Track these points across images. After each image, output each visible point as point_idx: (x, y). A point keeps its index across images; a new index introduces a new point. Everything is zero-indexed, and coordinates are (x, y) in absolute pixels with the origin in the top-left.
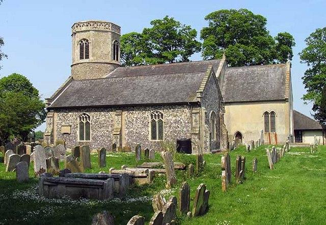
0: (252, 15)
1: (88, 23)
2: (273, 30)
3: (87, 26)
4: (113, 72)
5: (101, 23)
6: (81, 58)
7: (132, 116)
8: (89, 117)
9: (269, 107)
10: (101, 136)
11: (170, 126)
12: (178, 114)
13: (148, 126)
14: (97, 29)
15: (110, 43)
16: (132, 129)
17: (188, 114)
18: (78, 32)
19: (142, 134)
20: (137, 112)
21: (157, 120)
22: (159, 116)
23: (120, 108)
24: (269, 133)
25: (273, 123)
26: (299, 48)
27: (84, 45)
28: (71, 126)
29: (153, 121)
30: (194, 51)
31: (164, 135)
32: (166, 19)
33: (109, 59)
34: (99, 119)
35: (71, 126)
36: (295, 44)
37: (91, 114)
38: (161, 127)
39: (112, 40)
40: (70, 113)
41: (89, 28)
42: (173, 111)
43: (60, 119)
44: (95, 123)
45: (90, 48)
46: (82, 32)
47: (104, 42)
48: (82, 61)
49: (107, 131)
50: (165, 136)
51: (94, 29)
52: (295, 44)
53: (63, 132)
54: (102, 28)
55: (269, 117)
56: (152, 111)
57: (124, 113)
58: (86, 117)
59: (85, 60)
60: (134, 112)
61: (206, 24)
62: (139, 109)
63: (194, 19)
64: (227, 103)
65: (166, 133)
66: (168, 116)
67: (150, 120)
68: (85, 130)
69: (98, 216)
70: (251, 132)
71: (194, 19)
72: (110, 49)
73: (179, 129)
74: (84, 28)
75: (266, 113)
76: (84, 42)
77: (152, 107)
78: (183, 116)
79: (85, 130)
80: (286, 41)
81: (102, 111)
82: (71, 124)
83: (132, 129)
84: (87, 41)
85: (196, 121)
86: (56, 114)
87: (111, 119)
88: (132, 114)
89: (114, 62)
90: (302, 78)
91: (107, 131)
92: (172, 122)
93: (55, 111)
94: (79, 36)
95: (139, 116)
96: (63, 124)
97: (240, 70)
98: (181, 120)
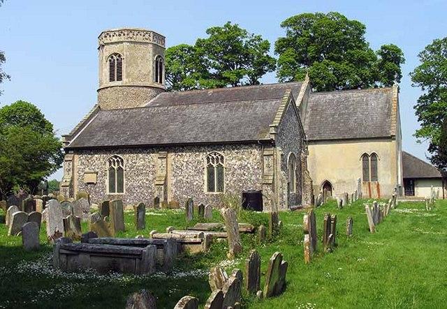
0: (346, 21)
1: (121, 32)
2: (375, 41)
3: (120, 35)
4: (154, 99)
5: (139, 31)
6: (112, 79)
7: (181, 159)
8: (122, 161)
9: (369, 147)
10: (139, 187)
11: (233, 173)
12: (244, 156)
13: (202, 173)
14: (133, 40)
15: (151, 59)
16: (181, 177)
17: (258, 157)
18: (107, 44)
19: (195, 184)
20: (188, 154)
21: (215, 165)
22: (217, 159)
23: (164, 148)
24: (369, 183)
25: (375, 169)
26: (409, 66)
27: (116, 61)
28: (97, 173)
29: (210, 167)
30: (266, 71)
31: (225, 185)
32: (227, 26)
33: (150, 81)
34: (135, 163)
35: (97, 173)
36: (404, 60)
37: (125, 157)
38: (221, 174)
39: (154, 56)
40: (96, 156)
41: (122, 38)
42: (237, 153)
43: (82, 164)
44: (131, 168)
45: (124, 66)
46: (112, 43)
47: (143, 58)
48: (112, 84)
49: (147, 180)
50: (227, 187)
51: (129, 40)
52: (404, 60)
53: (86, 182)
54: (140, 38)
55: (370, 161)
56: (208, 153)
57: (169, 155)
58: (118, 161)
59: (116, 83)
60: (184, 154)
61: (283, 33)
62: (190, 150)
63: (266, 27)
64: (311, 142)
65: (227, 182)
66: (231, 159)
67: (206, 165)
68: (117, 178)
69: (135, 296)
70: (344, 182)
71: (266, 27)
72: (151, 68)
73: (245, 177)
74: (115, 39)
75: (365, 155)
76: (115, 58)
77: (208, 147)
78: (251, 159)
79: (117, 178)
80: (392, 56)
81: (140, 152)
82: (97, 170)
83: (181, 177)
84: (120, 56)
85: (268, 166)
86: (77, 157)
87: (153, 164)
88: (181, 156)
89: (156, 85)
90: (415, 107)
91: (147, 180)
92: (236, 167)
93: (75, 153)
94: (109, 50)
95: (191, 160)
96: (87, 170)
97: (329, 96)
98: (249, 165)
